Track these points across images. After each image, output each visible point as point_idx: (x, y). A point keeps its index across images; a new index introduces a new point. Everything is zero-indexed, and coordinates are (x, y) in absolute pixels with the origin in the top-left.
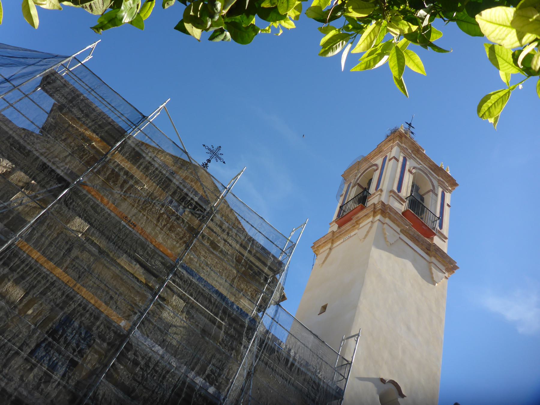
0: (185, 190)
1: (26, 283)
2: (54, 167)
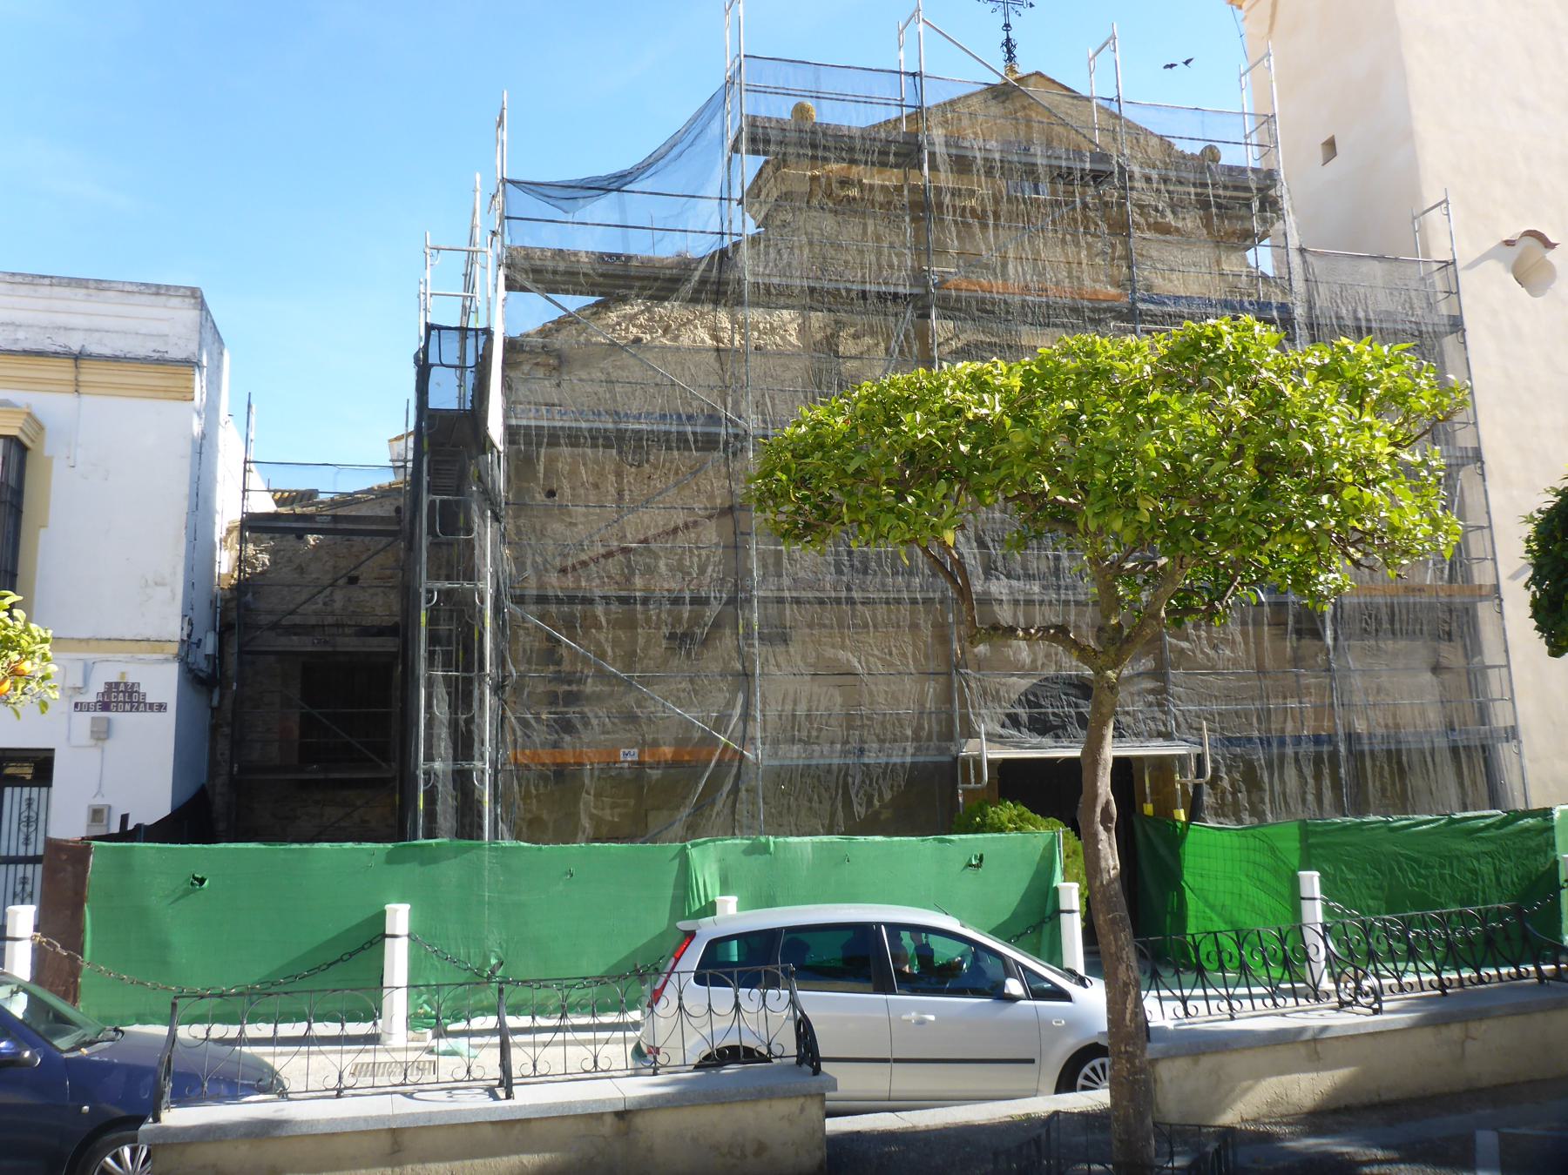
0: (1064, 164)
1: (557, 417)
2: (892, 289)
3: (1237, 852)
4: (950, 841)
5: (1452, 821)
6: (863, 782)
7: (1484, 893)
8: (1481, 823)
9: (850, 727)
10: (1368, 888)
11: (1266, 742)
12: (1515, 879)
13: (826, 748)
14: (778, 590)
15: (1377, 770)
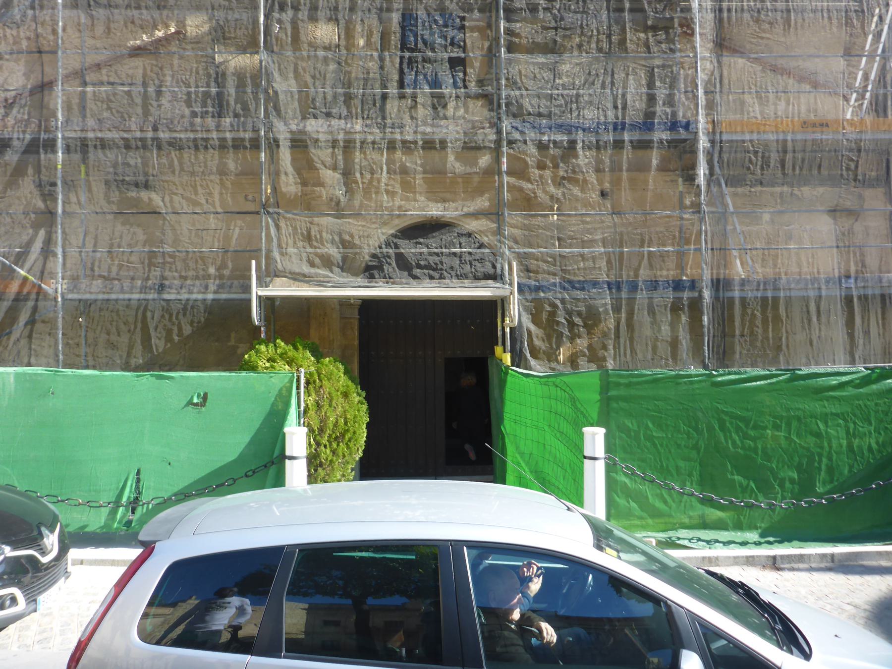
3: (541, 400)
4: (172, 378)
5: (796, 378)
6: (163, 316)
7: (830, 459)
8: (834, 381)
9: (151, 264)
10: (679, 446)
11: (615, 286)
12: (874, 446)
13: (127, 284)
14: (82, 131)
15: (748, 318)
